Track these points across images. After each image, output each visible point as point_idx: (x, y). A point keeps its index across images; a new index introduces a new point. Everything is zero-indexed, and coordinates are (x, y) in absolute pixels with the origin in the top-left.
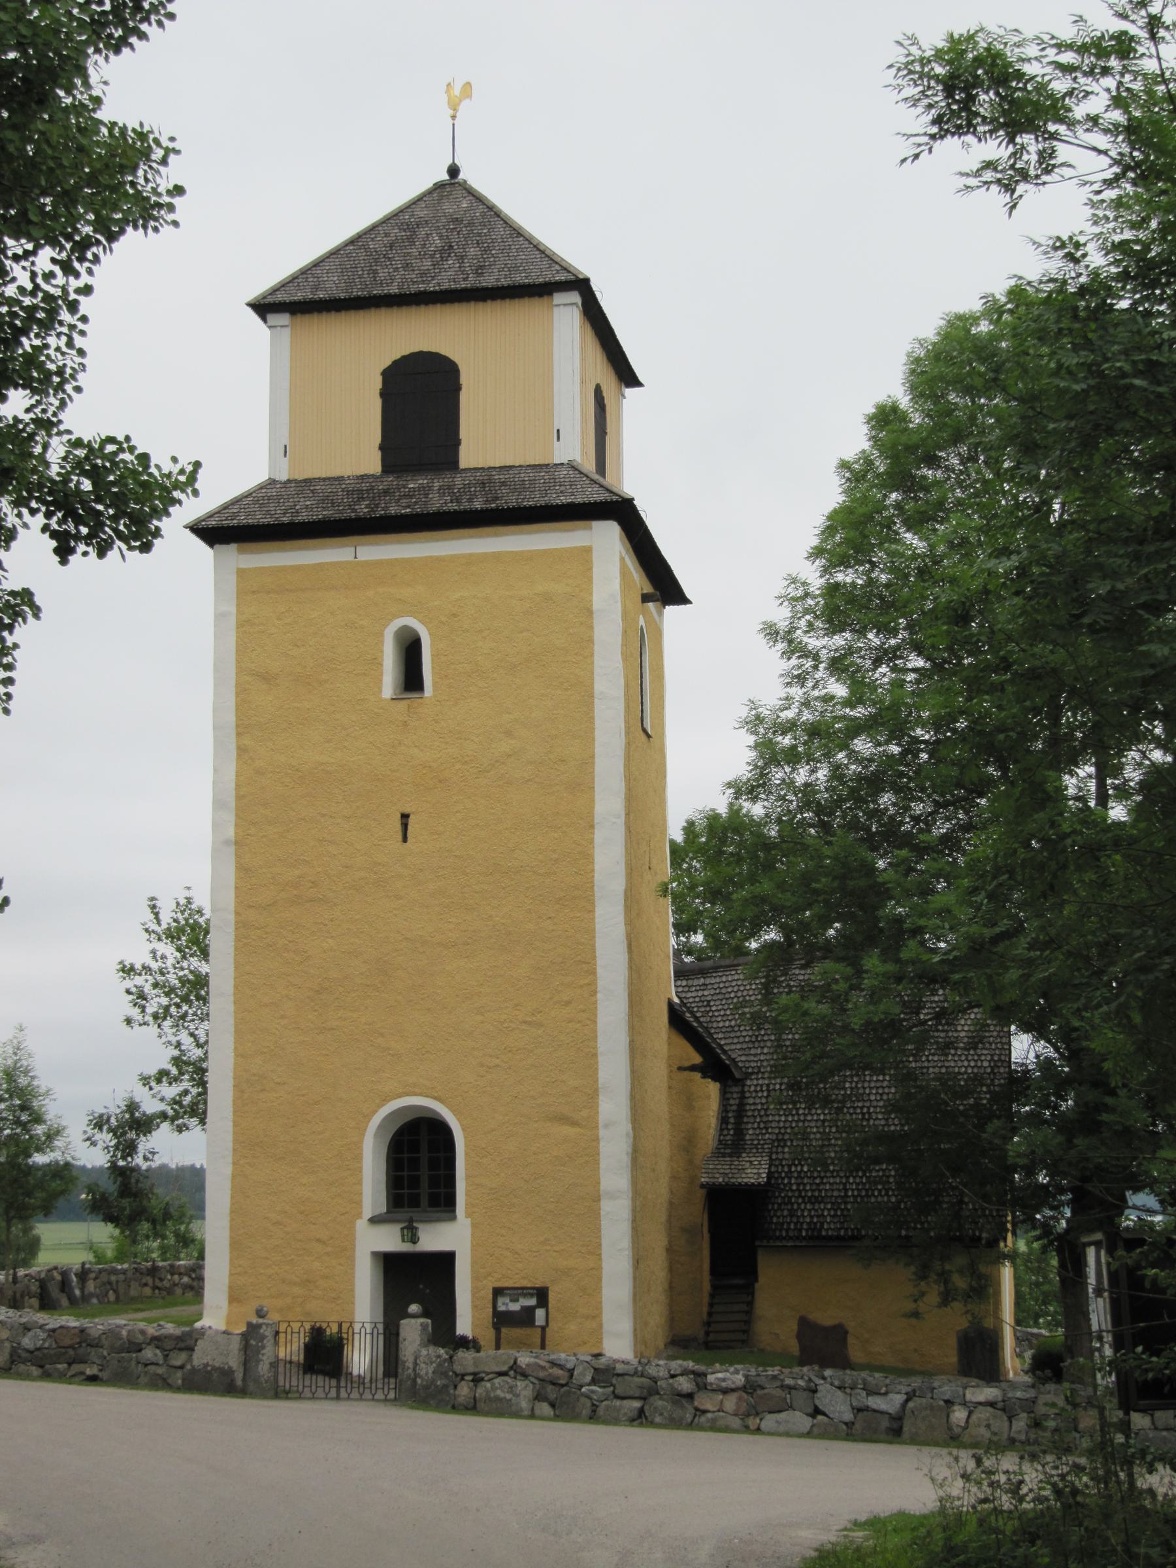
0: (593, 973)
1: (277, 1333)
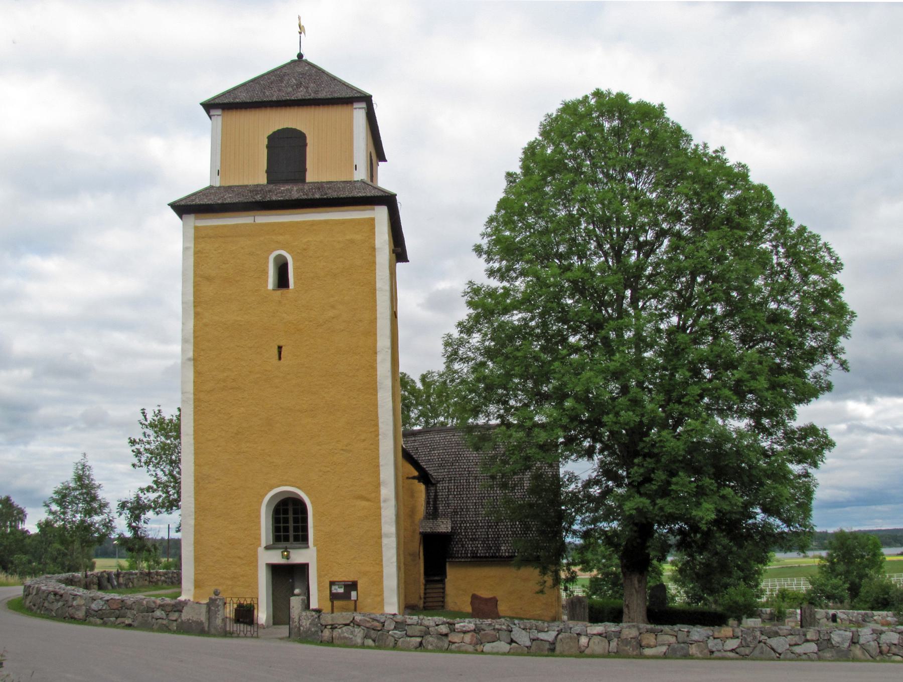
0: (377, 425)
1: (225, 603)
